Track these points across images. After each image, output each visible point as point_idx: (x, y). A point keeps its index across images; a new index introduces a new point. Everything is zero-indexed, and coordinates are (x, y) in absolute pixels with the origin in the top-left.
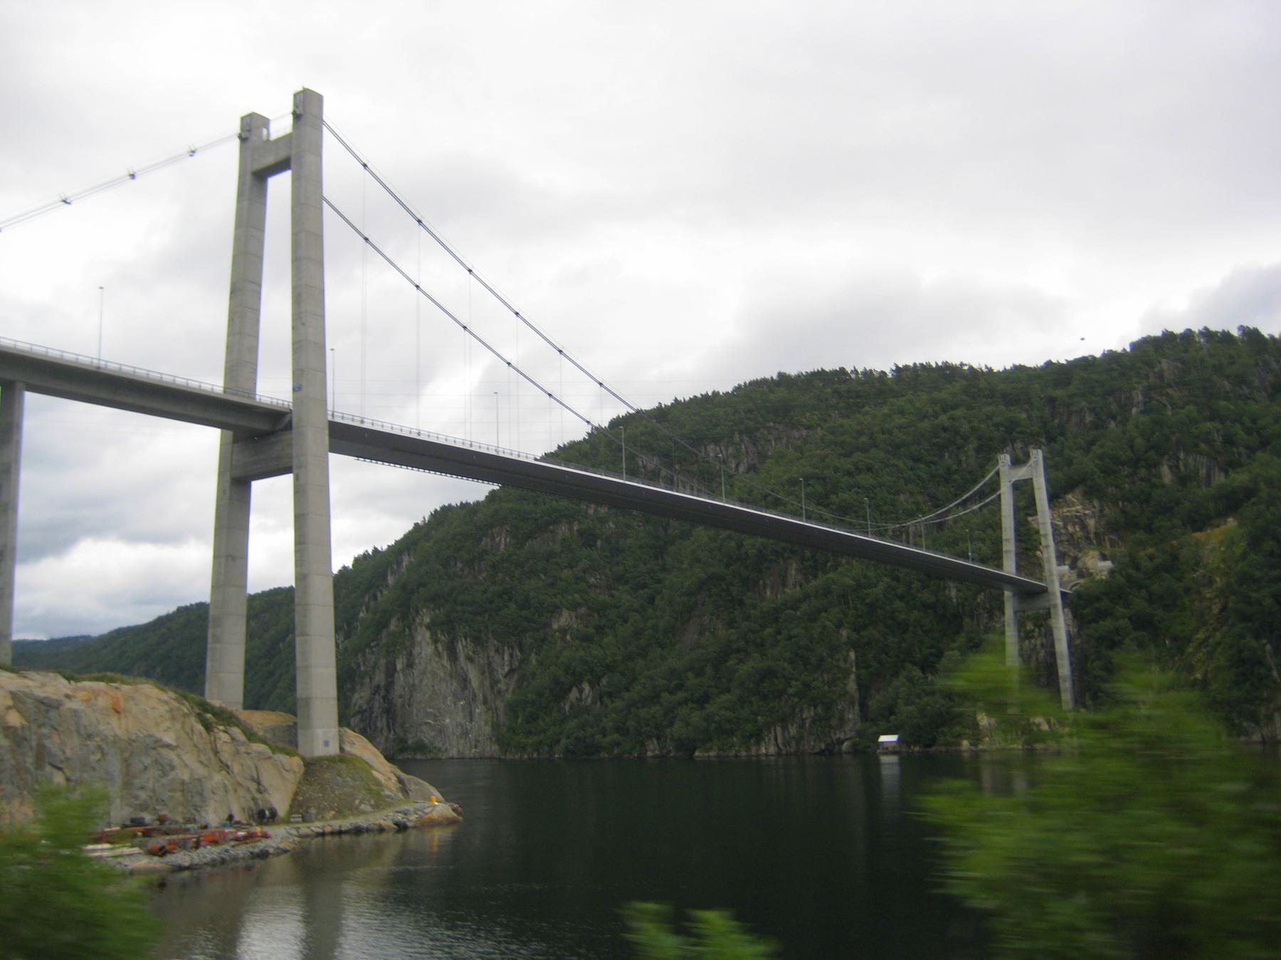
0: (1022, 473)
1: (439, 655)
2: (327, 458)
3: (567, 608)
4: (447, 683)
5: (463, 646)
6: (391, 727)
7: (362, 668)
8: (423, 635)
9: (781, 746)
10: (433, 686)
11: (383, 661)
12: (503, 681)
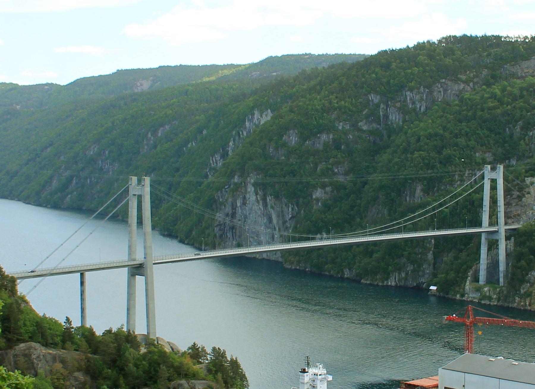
0: (493, 175)
1: (258, 202)
2: (153, 266)
3: (320, 188)
4: (262, 218)
5: (269, 199)
6: (234, 237)
7: (221, 200)
8: (251, 189)
9: (397, 282)
10: (255, 218)
11: (230, 200)
12: (288, 222)
